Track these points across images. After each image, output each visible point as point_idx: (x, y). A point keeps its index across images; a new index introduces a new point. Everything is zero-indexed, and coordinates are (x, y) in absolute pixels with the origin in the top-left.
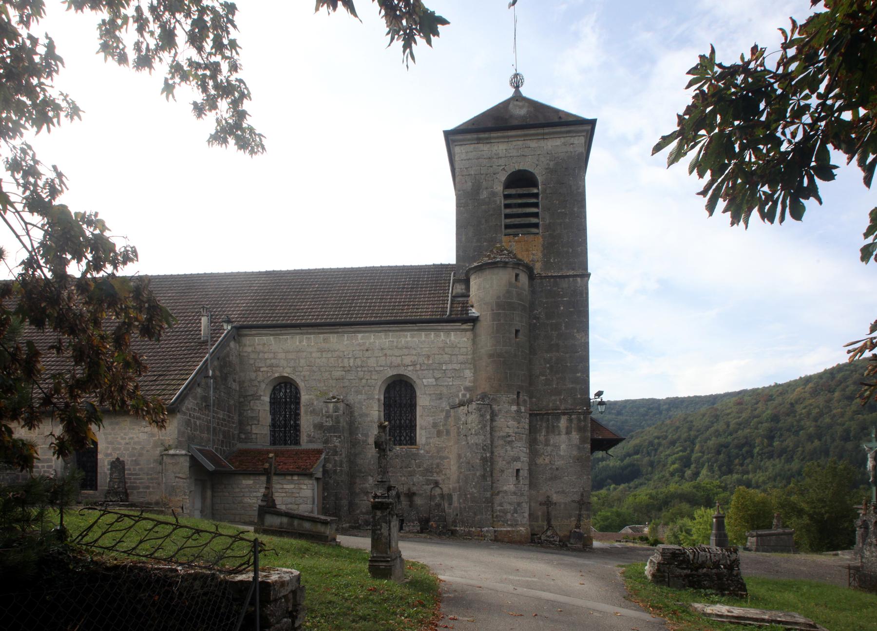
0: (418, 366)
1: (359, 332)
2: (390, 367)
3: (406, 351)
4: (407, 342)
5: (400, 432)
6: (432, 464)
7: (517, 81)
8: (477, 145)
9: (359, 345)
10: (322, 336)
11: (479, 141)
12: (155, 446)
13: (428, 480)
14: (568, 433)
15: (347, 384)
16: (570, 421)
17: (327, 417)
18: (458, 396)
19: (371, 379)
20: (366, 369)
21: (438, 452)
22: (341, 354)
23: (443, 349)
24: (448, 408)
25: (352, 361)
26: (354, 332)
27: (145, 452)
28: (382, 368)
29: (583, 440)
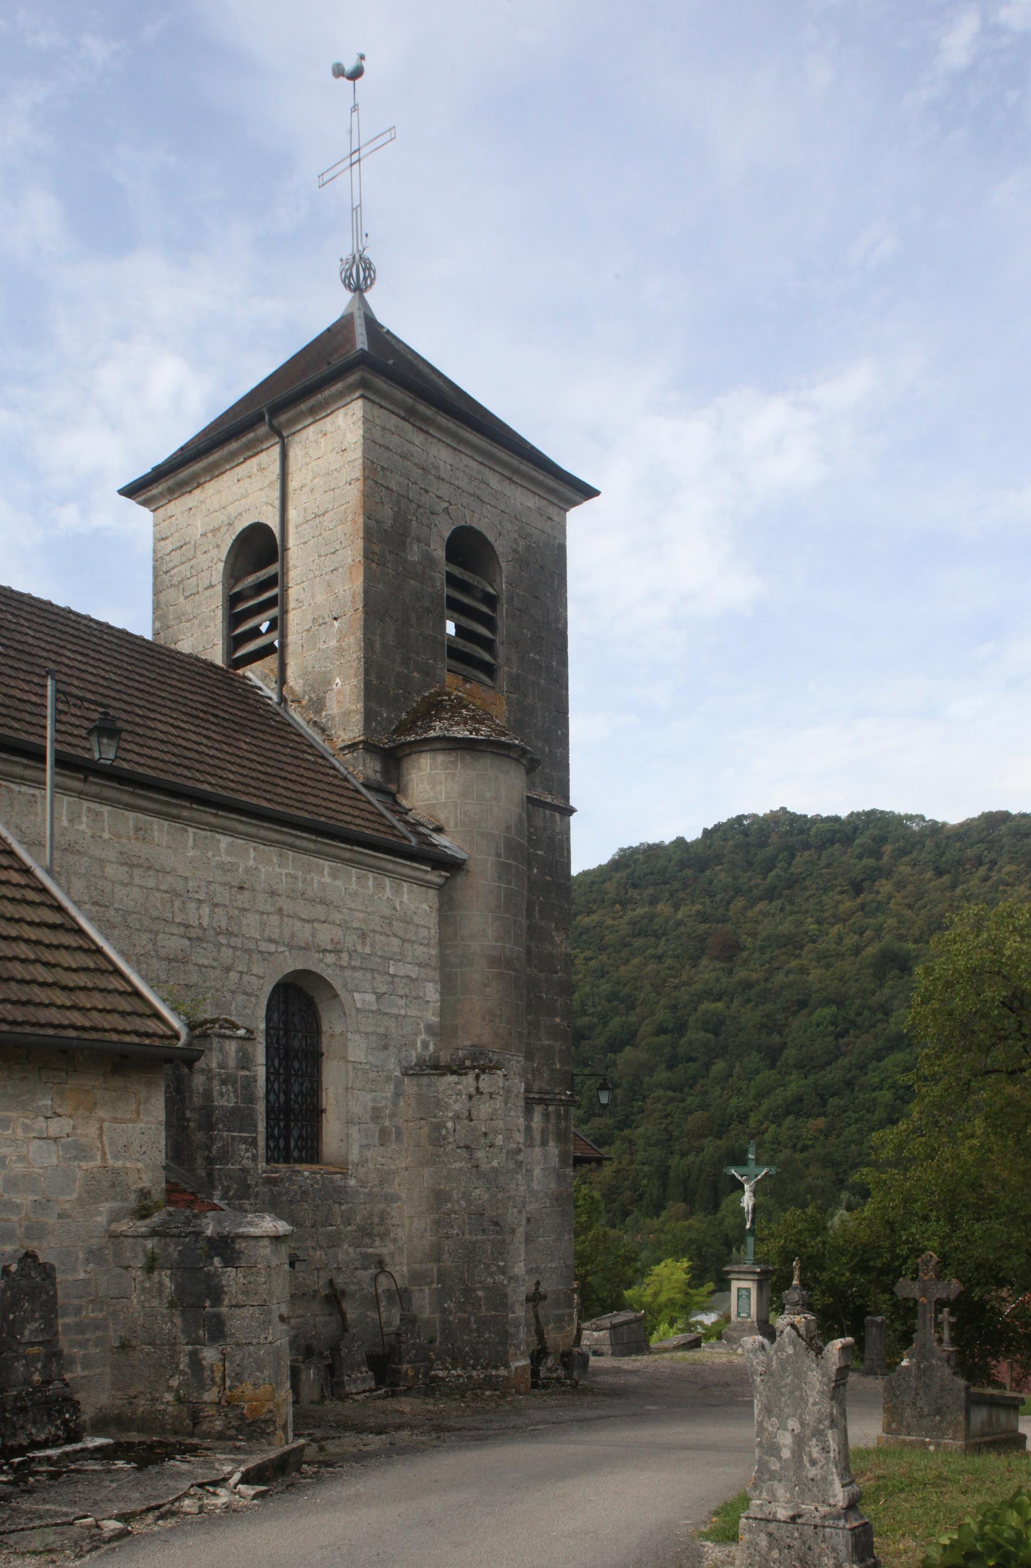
0: (345, 956)
1: (225, 831)
2: (290, 947)
3: (320, 911)
4: (323, 887)
5: (287, 1127)
6: (371, 1215)
7: (359, 277)
8: (401, 423)
9: (221, 866)
10: (131, 815)
11: (410, 415)
12: (91, 1196)
13: (365, 1256)
14: (544, 1143)
15: (194, 978)
16: (546, 1115)
17: (224, 1082)
18: (414, 1044)
19: (249, 972)
20: (237, 942)
21: (382, 1182)
22: (179, 886)
23: (388, 920)
24: (398, 1073)
25: (206, 910)
26: (213, 828)
27: (51, 1220)
28: (272, 948)
29: (563, 1156)
